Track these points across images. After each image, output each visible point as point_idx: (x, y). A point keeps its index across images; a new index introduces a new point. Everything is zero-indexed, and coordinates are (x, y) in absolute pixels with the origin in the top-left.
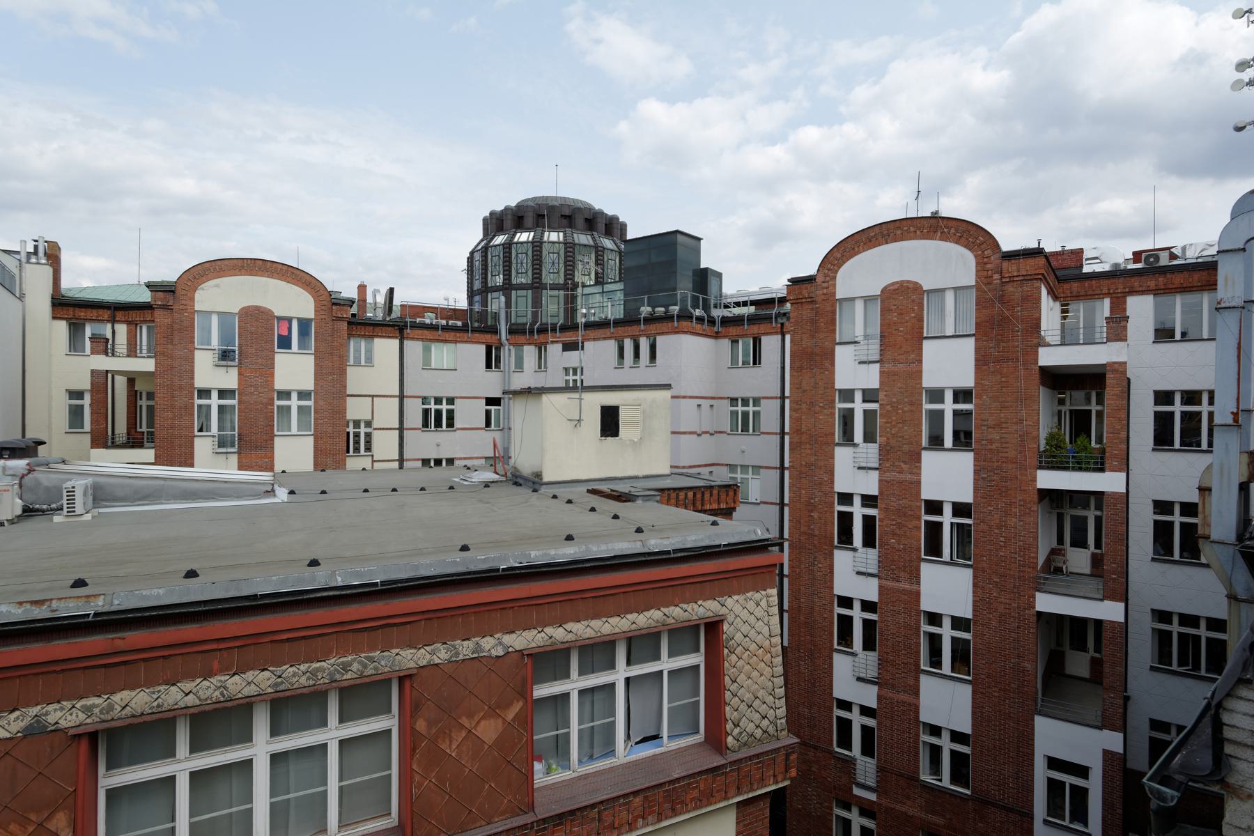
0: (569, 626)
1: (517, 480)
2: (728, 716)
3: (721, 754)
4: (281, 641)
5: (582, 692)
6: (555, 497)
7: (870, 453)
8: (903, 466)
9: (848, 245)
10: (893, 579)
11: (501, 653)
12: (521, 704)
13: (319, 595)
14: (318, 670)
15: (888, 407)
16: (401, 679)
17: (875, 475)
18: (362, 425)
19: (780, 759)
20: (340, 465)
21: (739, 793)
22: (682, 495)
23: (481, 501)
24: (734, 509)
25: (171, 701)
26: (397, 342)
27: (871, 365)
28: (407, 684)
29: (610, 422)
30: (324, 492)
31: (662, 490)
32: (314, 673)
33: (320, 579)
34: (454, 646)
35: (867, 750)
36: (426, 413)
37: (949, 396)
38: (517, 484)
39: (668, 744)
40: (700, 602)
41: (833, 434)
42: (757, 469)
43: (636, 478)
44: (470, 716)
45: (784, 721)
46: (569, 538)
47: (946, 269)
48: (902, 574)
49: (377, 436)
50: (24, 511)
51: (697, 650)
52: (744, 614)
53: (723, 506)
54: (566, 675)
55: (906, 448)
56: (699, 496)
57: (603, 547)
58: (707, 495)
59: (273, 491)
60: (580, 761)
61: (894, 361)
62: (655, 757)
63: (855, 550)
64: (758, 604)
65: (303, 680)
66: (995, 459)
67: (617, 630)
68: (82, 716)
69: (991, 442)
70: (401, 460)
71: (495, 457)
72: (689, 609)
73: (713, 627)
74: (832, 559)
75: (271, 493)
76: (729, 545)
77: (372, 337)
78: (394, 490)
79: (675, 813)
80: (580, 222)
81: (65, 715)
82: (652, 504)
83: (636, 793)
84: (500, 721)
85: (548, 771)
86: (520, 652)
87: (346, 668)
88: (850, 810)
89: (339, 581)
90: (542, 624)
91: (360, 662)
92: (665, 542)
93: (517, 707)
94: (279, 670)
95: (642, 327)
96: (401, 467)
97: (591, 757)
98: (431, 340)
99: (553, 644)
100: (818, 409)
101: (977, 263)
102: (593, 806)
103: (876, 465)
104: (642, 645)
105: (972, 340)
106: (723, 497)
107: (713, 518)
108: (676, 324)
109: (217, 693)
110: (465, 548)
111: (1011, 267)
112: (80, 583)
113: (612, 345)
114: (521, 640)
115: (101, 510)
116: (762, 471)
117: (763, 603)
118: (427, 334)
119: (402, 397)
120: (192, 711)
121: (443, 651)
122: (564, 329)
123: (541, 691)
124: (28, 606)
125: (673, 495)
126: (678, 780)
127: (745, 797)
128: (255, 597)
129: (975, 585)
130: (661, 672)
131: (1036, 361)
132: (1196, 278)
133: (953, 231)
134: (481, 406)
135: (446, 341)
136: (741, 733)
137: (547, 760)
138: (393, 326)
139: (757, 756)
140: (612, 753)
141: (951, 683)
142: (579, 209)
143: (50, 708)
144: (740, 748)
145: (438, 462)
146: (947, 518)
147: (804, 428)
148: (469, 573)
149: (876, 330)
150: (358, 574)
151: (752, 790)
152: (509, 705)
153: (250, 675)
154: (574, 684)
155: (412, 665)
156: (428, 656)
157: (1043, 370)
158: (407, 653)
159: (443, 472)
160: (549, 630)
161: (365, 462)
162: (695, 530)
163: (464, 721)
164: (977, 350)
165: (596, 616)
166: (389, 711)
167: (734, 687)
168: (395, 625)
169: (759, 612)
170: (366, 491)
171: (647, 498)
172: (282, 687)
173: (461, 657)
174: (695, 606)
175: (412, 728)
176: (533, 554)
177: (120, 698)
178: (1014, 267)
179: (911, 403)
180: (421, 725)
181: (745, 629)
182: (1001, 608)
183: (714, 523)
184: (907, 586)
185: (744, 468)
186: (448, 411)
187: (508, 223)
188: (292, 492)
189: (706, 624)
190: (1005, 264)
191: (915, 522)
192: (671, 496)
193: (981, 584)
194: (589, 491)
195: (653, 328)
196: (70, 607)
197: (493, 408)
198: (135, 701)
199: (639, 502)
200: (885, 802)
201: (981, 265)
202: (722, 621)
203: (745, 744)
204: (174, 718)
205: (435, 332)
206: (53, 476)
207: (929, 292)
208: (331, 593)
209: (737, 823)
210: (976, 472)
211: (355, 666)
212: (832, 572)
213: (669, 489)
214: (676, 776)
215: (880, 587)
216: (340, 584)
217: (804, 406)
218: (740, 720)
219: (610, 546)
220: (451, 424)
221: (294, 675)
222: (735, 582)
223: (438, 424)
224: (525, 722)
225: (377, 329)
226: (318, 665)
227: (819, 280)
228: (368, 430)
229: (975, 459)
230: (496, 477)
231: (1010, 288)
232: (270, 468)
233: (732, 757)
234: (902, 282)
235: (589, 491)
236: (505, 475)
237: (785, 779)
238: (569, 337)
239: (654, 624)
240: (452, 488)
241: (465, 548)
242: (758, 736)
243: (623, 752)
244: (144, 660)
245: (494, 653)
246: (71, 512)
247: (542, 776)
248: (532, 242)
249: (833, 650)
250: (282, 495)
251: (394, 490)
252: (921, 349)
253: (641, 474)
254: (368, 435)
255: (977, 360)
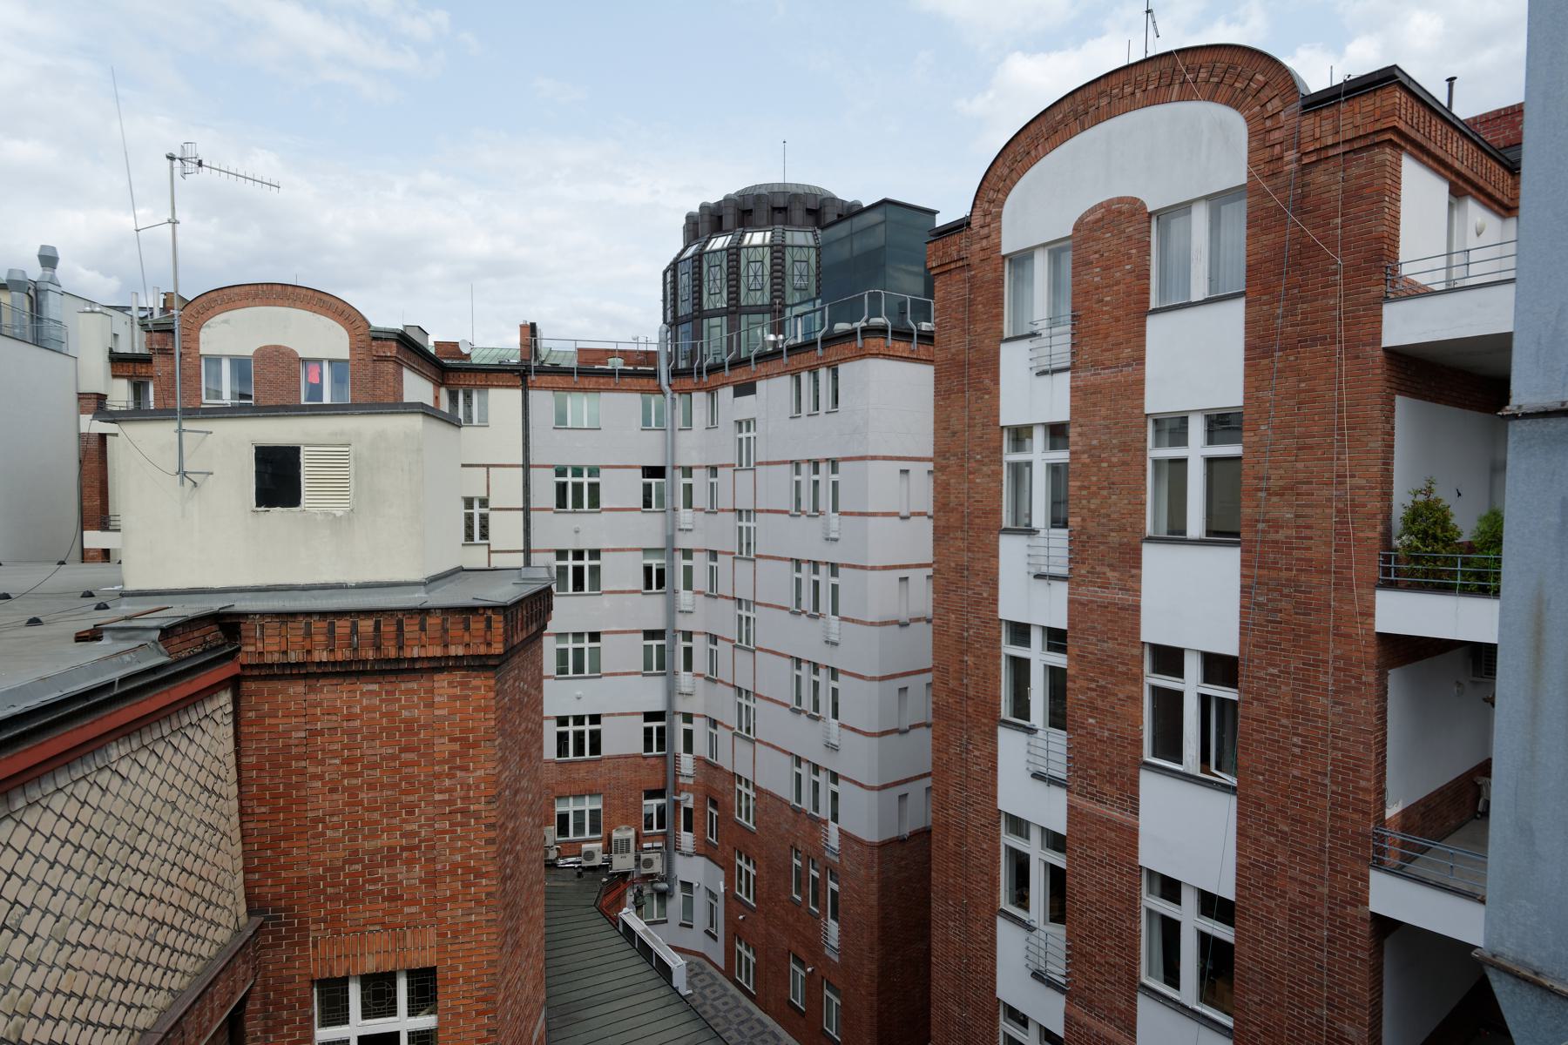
7: (1055, 546)
8: (1110, 574)
9: (1020, 148)
10: (1092, 796)
15: (1085, 458)
17: (1061, 591)
18: (476, 504)
22: (343, 627)
26: (518, 393)
27: (1057, 376)
29: (278, 478)
36: (561, 488)
37: (1197, 429)
41: (998, 512)
47: (1195, 155)
48: (1107, 788)
49: (494, 518)
55: (1114, 538)
61: (1095, 364)
63: (1031, 731)
66: (1282, 563)
69: (1276, 525)
70: (527, 551)
74: (995, 743)
77: (487, 387)
80: (798, 214)
95: (820, 352)
96: (527, 563)
98: (564, 389)
100: (973, 464)
101: (1252, 134)
103: (1064, 571)
105: (1239, 306)
108: (860, 343)
111: (1320, 128)
113: (786, 382)
118: (559, 380)
119: (526, 466)
122: (735, 364)
129: (1241, 833)
131: (1377, 336)
133: (1203, 75)
134: (638, 480)
135: (585, 390)
138: (511, 371)
141: (1191, 1027)
142: (796, 196)
146: (1192, 685)
147: (953, 501)
149: (1066, 310)
157: (1396, 356)
164: (1250, 324)
178: (1327, 126)
179: (1124, 448)
182: (1293, 891)
184: (1116, 814)
186: (590, 485)
187: (704, 227)
190: (1309, 123)
191: (1131, 688)
193: (1252, 832)
195: (835, 352)
197: (653, 481)
201: (1259, 137)
205: (569, 379)
207: (1158, 213)
210: (1245, 590)
212: (994, 768)
215: (1070, 808)
217: (953, 461)
220: (595, 502)
223: (578, 503)
225: (492, 376)
227: (975, 224)
228: (484, 511)
229: (1245, 564)
231: (1319, 177)
234: (1110, 202)
238: (741, 375)
248: (727, 249)
252: (1142, 335)
253: (352, 578)
254: (484, 519)
255: (1249, 347)
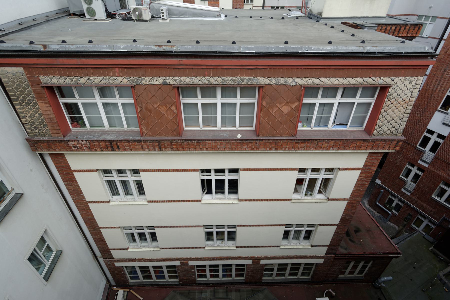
0: (322, 79)
1: (310, 16)
2: (377, 123)
3: (369, 136)
4: (224, 68)
5: (321, 104)
6: (326, 25)
11: (294, 85)
12: (298, 103)
13: (235, 54)
14: (235, 80)
16: (259, 87)
19: (394, 143)
20: (241, 7)
21: (372, 148)
22: (389, 28)
23: (294, 24)
24: (415, 37)
25: (195, 82)
28: (261, 89)
30: (236, 17)
31: (379, 24)
32: (233, 81)
33: (236, 48)
34: (278, 79)
35: (433, 150)
38: (310, 18)
39: (348, 128)
40: (381, 78)
42: (434, 18)
43: (367, 18)
44: (280, 104)
45: (402, 130)
46: (330, 42)
50: (152, 17)
51: (373, 97)
52: (402, 86)
53: (409, 35)
54: (316, 97)
56: (398, 29)
57: (344, 48)
58: (402, 29)
59: (220, 15)
60: (314, 126)
62: (342, 131)
64: (410, 83)
65: (230, 82)
67: (341, 83)
68: (175, 82)
70: (263, 7)
71: (302, 7)
72: (376, 80)
73: (384, 89)
75: (219, 16)
76: (408, 53)
78: (261, 17)
79: (344, 149)
81: (172, 81)
82: (372, 31)
83: (332, 140)
84: (290, 107)
85: (303, 126)
86: (301, 86)
87: (243, 80)
88: (413, 167)
89: (242, 50)
90: (311, 76)
91: (247, 80)
92: (375, 49)
93: (297, 104)
94: (224, 78)
97: (319, 126)
99: (314, 84)
102: (316, 140)
104: (349, 91)
106: (411, 30)
107: (402, 40)
109: (207, 82)
110: (286, 43)
112: (169, 42)
114: (302, 81)
115: (171, 19)
116: (437, 19)
117: (414, 83)
120: (201, 86)
121: (274, 81)
123: (305, 101)
124: (158, 47)
125: (384, 27)
126: (349, 140)
127: (374, 151)
128: (216, 52)
130: (354, 103)
132: (47, 278)
136: (381, 131)
137: (303, 123)
139: (385, 139)
140: (327, 126)
143: (168, 78)
144: (378, 135)
145: (278, 8)
148: (287, 53)
150: (248, 48)
151: (377, 150)
152: (293, 103)
153: (216, 78)
154: (319, 100)
155: (263, 83)
156: (269, 81)
158: (262, 79)
159: (279, 11)
160: (313, 79)
161: (251, 6)
162: (392, 44)
163: (278, 105)
165: (333, 77)
166: (255, 97)
167: (384, 114)
168: (259, 69)
169: (409, 86)
170: (251, 17)
171: (370, 28)
172: (224, 83)
173: (280, 84)
174: (379, 79)
175: (262, 104)
176: (313, 48)
177: (183, 78)
180: (264, 103)
181: (399, 92)
183: (403, 42)
185: (427, 17)
188: (226, 16)
189: (381, 87)
192: (384, 28)
194: (342, 23)
196: (167, 49)
198: (186, 80)
199: (366, 29)
200: (431, 168)
202: (390, 87)
203: (381, 134)
204: (196, 87)
206: (157, 5)
208: (239, 54)
209: (367, 158)
211: (246, 81)
213: (383, 24)
214: (349, 138)
216: (242, 51)
218: (382, 126)
219: (347, 48)
221: (228, 80)
222: (403, 71)
224: (298, 109)
226: (235, 78)
230: (301, 14)
232: (218, 6)
233: (373, 137)
235: (342, 23)
236: (306, 14)
237: (393, 150)
239: (357, 83)
240: (283, 18)
241: (286, 43)
242: (388, 133)
243: (331, 126)
244: (188, 68)
245: (291, 84)
246: (163, 19)
247: (300, 127)
249: (436, 110)
250: (223, 17)
251: (261, 17)
253: (370, 15)
